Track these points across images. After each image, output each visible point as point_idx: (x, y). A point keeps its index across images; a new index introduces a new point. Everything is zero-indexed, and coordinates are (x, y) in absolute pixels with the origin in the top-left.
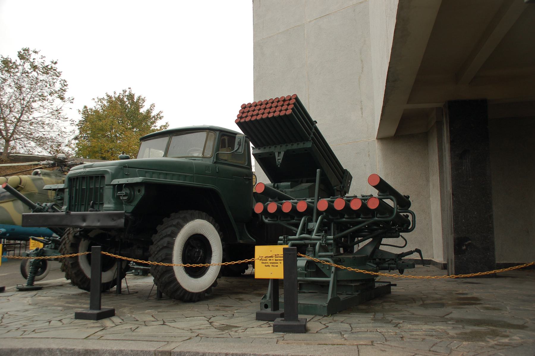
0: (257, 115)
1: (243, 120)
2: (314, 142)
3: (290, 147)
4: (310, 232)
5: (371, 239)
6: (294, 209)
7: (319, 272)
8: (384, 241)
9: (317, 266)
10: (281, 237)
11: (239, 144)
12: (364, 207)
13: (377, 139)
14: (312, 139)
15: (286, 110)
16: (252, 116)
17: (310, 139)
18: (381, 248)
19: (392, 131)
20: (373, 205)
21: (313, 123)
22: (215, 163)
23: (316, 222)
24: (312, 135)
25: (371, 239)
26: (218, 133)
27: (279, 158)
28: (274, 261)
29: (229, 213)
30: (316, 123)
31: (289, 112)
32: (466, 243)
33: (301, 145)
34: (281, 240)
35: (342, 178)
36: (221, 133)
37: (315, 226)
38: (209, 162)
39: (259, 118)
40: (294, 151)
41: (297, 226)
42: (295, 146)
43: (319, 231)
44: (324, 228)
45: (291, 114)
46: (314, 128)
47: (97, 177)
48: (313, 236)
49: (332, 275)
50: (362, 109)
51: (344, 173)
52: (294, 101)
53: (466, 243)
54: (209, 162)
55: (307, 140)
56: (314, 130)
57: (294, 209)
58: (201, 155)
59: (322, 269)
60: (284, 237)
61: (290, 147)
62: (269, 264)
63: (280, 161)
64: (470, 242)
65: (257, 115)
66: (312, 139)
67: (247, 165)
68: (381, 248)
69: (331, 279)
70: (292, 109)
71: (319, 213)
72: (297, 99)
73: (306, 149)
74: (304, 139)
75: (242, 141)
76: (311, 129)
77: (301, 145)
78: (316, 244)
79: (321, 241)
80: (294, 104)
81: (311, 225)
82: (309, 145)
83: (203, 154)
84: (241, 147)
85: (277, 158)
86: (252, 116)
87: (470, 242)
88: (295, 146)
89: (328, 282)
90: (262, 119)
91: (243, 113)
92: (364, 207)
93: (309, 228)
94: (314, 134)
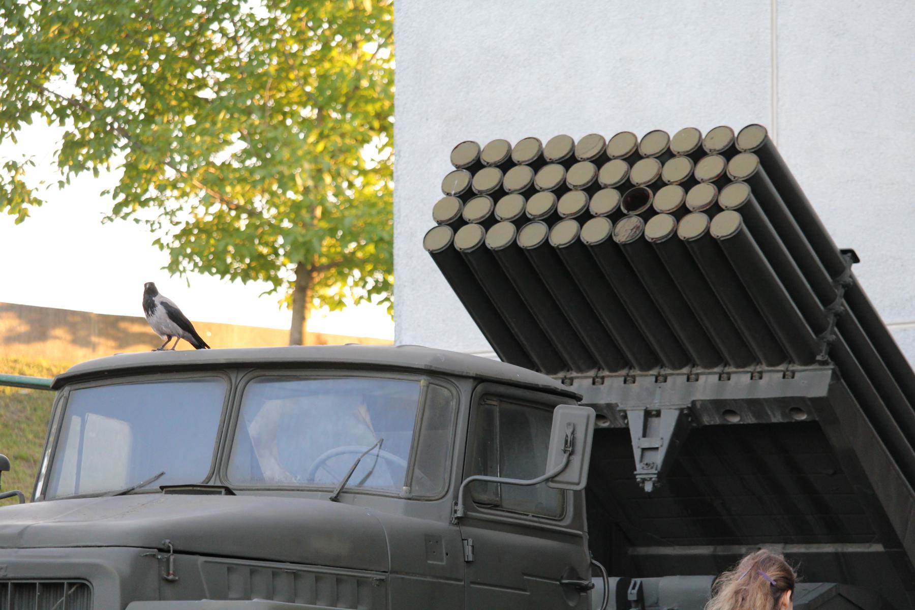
1: (467, 239)
2: (843, 373)
3: (707, 386)
11: (570, 446)
15: (713, 210)
21: (840, 261)
22: (460, 521)
24: (833, 334)
26: (465, 389)
27: (646, 443)
30: (856, 260)
31: (726, 225)
36: (480, 388)
38: (437, 518)
42: (740, 384)
45: (737, 238)
47: (52, 587)
52: (745, 165)
54: (437, 518)
56: (841, 305)
63: (658, 458)
70: (744, 210)
72: (766, 154)
75: (580, 435)
80: (753, 181)
84: (576, 459)
85: (637, 442)
88: (740, 384)
91: (467, 195)
94: (842, 323)
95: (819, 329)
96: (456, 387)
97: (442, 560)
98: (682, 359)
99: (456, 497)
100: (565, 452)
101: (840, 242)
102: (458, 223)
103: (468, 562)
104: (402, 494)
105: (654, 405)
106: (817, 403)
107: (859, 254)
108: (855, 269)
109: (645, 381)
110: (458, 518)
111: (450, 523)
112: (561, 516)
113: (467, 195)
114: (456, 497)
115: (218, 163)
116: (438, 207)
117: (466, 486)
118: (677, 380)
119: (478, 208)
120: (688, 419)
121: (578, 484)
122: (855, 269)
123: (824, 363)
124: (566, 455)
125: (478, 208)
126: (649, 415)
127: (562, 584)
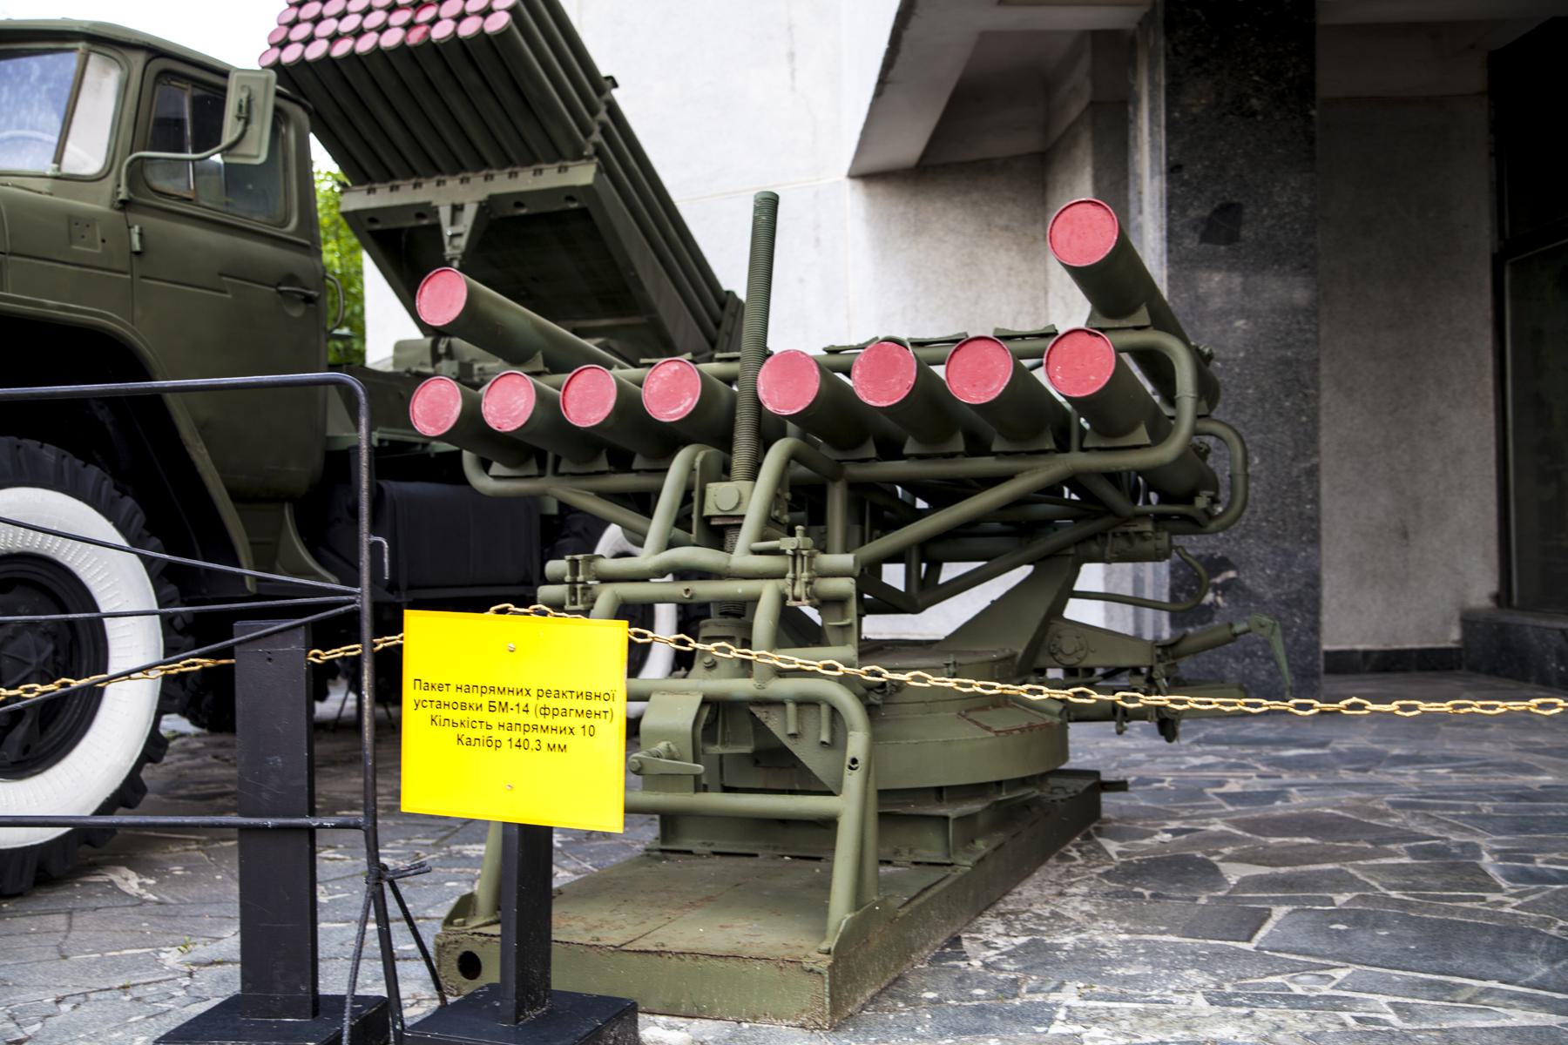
0: (359, 33)
1: (290, 55)
2: (605, 168)
3: (502, 184)
4: (718, 533)
5: (1026, 570)
6: (629, 405)
7: (776, 764)
8: (1091, 576)
9: (760, 728)
10: (555, 567)
12: (1023, 390)
13: (852, 176)
14: (599, 152)
16: (335, 38)
17: (589, 151)
18: (1075, 610)
19: (908, 146)
20: (1059, 382)
22: (125, 205)
23: (753, 476)
24: (597, 137)
25: (1026, 570)
28: (530, 719)
29: (200, 455)
30: (615, 85)
32: (1218, 580)
33: (550, 178)
34: (559, 581)
35: (718, 325)
37: (748, 496)
38: (97, 204)
39: (365, 45)
40: (519, 199)
41: (644, 503)
42: (527, 181)
43: (773, 524)
44: (800, 503)
45: (504, 34)
46: (603, 108)
48: (740, 555)
49: (853, 782)
50: (792, 55)
51: (722, 306)
53: (1218, 580)
54: (97, 204)
55: (578, 156)
56: (603, 116)
57: (629, 405)
58: (49, 168)
59: (788, 743)
60: (574, 565)
61: (502, 184)
62: (497, 734)
63: (462, 242)
64: (1231, 574)
65: (359, 33)
66: (599, 152)
67: (297, 232)
68: (1075, 610)
69: (847, 806)
71: (768, 430)
73: (570, 193)
74: (560, 152)
75: (258, 101)
76: (593, 112)
77: (550, 178)
78: (754, 600)
79: (784, 584)
81: (720, 497)
82: (583, 174)
83: (58, 159)
84: (254, 127)
86: (335, 38)
87: (1231, 574)
88: (527, 181)
89: (828, 824)
90: (377, 50)
91: (292, 25)
92: (1023, 390)
93: (710, 510)
94: (605, 131)
95: (587, 133)
96: (127, 61)
97: (95, 247)
98: (481, 164)
99: (118, 178)
100: (239, 118)
101: (604, 71)
102: (284, 44)
103: (137, 253)
104: (49, 173)
105: (458, 201)
106: (586, 189)
107: (618, 80)
108: (615, 92)
109: (452, 183)
110: (122, 202)
111: (112, 206)
112: (284, 224)
113: (292, 25)
114: (118, 178)
115: (1078, 759)
116: (271, 35)
117: (130, 165)
118: (477, 180)
119: (302, 31)
120: (487, 207)
121: (257, 157)
122: (615, 92)
123: (589, 158)
124: (242, 122)
125: (302, 31)
126: (457, 209)
127: (281, 292)
